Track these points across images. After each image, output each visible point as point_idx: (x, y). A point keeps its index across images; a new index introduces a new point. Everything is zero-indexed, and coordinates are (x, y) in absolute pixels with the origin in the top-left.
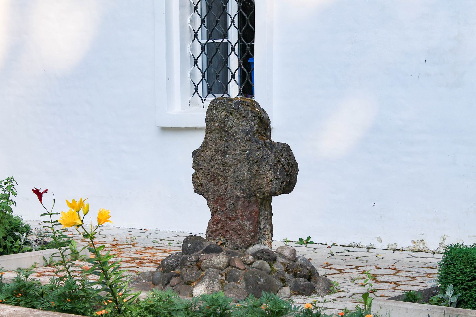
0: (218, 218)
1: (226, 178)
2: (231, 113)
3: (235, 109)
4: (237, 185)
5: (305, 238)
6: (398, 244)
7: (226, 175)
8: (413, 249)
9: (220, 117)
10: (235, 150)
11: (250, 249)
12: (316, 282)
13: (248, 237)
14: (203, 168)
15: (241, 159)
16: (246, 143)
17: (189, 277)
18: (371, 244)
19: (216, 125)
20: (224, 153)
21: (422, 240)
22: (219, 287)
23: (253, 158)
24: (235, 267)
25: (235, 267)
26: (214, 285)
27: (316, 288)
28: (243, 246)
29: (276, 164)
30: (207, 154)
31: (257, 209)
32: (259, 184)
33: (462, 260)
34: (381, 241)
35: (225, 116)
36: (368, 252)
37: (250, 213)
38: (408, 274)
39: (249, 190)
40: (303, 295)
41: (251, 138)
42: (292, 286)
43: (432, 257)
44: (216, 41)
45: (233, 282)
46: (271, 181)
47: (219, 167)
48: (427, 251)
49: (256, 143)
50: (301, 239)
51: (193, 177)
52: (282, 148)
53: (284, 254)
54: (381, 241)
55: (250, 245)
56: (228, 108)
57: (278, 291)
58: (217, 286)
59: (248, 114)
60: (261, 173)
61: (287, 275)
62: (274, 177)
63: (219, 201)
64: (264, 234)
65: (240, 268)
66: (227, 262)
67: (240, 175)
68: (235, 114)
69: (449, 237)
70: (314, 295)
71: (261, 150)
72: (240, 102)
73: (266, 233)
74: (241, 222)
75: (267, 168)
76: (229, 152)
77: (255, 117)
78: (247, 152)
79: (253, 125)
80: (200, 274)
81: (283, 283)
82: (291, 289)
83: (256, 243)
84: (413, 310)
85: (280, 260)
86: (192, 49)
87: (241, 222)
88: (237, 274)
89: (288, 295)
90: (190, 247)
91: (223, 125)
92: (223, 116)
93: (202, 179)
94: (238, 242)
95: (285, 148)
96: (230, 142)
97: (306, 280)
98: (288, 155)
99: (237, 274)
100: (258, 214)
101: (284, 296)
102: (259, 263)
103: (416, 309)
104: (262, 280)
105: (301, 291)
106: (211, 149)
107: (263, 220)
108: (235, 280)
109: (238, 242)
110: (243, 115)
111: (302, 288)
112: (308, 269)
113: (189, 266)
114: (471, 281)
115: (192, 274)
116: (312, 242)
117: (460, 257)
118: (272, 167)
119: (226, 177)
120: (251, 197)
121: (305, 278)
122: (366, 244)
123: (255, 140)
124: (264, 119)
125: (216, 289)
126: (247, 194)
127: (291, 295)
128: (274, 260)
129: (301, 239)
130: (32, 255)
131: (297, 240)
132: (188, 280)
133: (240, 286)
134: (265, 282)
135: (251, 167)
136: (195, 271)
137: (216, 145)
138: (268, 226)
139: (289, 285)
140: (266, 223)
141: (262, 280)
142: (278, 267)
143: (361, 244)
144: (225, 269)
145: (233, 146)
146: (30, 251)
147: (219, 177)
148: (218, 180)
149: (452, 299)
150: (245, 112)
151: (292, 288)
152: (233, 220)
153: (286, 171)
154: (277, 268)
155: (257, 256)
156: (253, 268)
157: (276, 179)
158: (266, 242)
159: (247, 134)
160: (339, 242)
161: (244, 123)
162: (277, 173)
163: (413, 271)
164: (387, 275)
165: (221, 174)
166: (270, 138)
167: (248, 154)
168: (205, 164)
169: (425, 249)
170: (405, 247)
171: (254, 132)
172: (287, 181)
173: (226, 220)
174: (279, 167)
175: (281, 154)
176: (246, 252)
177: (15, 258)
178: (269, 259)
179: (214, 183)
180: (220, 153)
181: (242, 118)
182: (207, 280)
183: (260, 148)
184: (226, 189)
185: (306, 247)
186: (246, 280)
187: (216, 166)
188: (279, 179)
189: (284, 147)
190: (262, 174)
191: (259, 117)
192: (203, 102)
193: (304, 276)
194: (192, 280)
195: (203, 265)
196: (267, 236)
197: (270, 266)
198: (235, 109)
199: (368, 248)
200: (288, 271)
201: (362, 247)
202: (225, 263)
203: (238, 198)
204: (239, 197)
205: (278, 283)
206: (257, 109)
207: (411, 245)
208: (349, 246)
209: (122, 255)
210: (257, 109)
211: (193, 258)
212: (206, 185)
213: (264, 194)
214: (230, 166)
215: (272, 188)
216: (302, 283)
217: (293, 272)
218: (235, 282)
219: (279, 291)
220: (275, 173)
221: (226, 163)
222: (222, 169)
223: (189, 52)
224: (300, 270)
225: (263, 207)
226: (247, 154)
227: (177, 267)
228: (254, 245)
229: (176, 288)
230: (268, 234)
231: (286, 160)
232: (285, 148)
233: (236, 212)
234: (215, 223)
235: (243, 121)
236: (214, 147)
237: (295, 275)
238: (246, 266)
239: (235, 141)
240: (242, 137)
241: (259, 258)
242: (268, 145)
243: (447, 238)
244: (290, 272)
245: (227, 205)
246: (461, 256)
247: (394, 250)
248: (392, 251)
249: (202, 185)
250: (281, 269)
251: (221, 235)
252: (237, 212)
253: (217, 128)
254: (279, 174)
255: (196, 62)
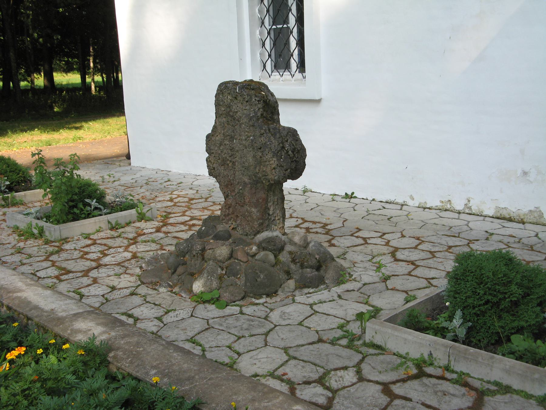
0: (229, 203)
1: (234, 163)
2: (236, 98)
3: (239, 94)
4: (244, 171)
5: (349, 193)
6: (428, 202)
7: (234, 160)
8: (441, 208)
9: (226, 101)
10: (240, 135)
11: (258, 236)
12: (326, 271)
13: (256, 224)
14: (214, 152)
15: (247, 145)
16: (250, 128)
17: (192, 268)
18: (404, 202)
19: (223, 109)
20: (232, 138)
21: (449, 201)
22: (217, 283)
23: (257, 143)
24: (238, 259)
25: (238, 259)
26: (211, 281)
27: (325, 277)
28: (251, 233)
29: (280, 151)
30: (217, 138)
31: (264, 196)
32: (264, 171)
33: (474, 275)
34: (413, 199)
35: (231, 100)
36: (401, 209)
37: (257, 200)
38: (429, 246)
39: (255, 176)
40: (309, 288)
41: (254, 123)
42: (297, 278)
43: (457, 218)
44: (278, 26)
45: (233, 277)
46: (274, 168)
47: (228, 152)
48: (453, 211)
49: (260, 128)
50: (346, 194)
51: (207, 160)
52: (288, 133)
53: (294, 240)
54: (413, 199)
55: (258, 232)
56: (232, 92)
57: (281, 285)
58: (215, 283)
59: (251, 98)
60: (265, 160)
61: (293, 266)
62: (277, 165)
63: (229, 187)
64: (274, 220)
65: (242, 260)
66: (229, 254)
67: (246, 161)
68: (239, 98)
69: (473, 199)
70: (322, 287)
71: (264, 136)
72: (244, 86)
73: (277, 218)
74: (249, 209)
75: (270, 155)
76: (236, 137)
77: (258, 101)
78: (251, 138)
79: (257, 109)
80: (203, 265)
81: (288, 275)
82: (296, 281)
83: (264, 230)
84: (413, 342)
85: (288, 248)
86: (261, 33)
87: (249, 209)
88: (238, 267)
89: (292, 289)
90: (203, 230)
91: (228, 110)
92: (229, 101)
93: (214, 163)
94: (247, 228)
95: (291, 132)
96: (236, 127)
97: (314, 270)
98: (294, 139)
99: (238, 267)
100: (266, 201)
101: (288, 290)
102: (262, 255)
103: (415, 342)
104: (262, 276)
105: (307, 284)
106: (220, 133)
107: (272, 206)
108: (235, 275)
109: (247, 228)
110: (246, 100)
111: (308, 280)
112: (316, 259)
113: (194, 256)
114: (484, 304)
115: (195, 265)
116: (355, 197)
117: (472, 272)
118: (275, 154)
119: (233, 162)
120: (257, 183)
121: (312, 269)
122: (401, 201)
123: (259, 126)
124: (271, 103)
125: (214, 285)
126: (254, 181)
127: (296, 289)
128: (282, 249)
129: (346, 194)
130: (97, 221)
131: (344, 194)
132: (191, 271)
133: (239, 283)
134: (265, 277)
135: (256, 153)
136: (199, 262)
137: (224, 130)
138: (278, 212)
139: (295, 277)
140: (275, 208)
141: (262, 276)
142: (284, 257)
143: (396, 201)
144: (226, 261)
145: (239, 131)
146: (101, 215)
147: (228, 162)
148: (228, 165)
149: (459, 329)
150: (248, 97)
151: (298, 280)
152: (242, 206)
153: (290, 158)
154: (283, 259)
155: (261, 247)
156: (256, 260)
157: (280, 167)
158: (276, 227)
159: (250, 119)
160: (378, 198)
161: (247, 108)
162: (280, 160)
163: (436, 241)
164: (409, 248)
165: (230, 159)
166: (279, 121)
167: (252, 140)
168: (216, 148)
169: (452, 209)
170: (434, 206)
171: (258, 117)
172: (292, 168)
173: (236, 206)
174: (283, 154)
175: (286, 139)
176: (254, 239)
177: (78, 224)
178: (274, 249)
179: (224, 167)
180: (228, 137)
181: (245, 102)
182: (205, 275)
183: (264, 134)
184: (234, 174)
185: (349, 202)
186: (246, 275)
187: (225, 151)
188: (282, 166)
189: (290, 132)
190: (266, 161)
191: (264, 101)
192: (270, 77)
193: (311, 267)
194: (195, 272)
195: (206, 256)
196: (278, 221)
197: (276, 257)
198: (239, 94)
199: (402, 205)
200: (295, 261)
201: (397, 204)
202: (226, 256)
203: (245, 184)
204: (246, 183)
205: (283, 276)
206: (263, 93)
207: (439, 204)
208: (387, 202)
209: (171, 221)
210: (263, 93)
211: (198, 247)
212: (217, 169)
213: (269, 181)
214: (237, 151)
215: (275, 176)
216: (309, 275)
217: (300, 263)
218: (234, 277)
219: (283, 286)
220: (278, 160)
221: (233, 148)
222: (230, 154)
223: (258, 36)
224: (308, 260)
225: (272, 193)
226: (251, 140)
227: (187, 253)
228: (262, 232)
229: (181, 278)
230: (279, 219)
231: (291, 146)
232: (291, 132)
233: (244, 199)
234: (227, 207)
235: (247, 106)
236: (222, 132)
237: (302, 266)
238: (249, 258)
239: (241, 125)
240: (246, 123)
241: (264, 249)
242: (271, 130)
243: (471, 200)
244: (297, 262)
245: (236, 191)
246: (474, 271)
247: (425, 208)
248: (422, 209)
249: (214, 169)
250: (287, 260)
251: (232, 219)
252: (245, 198)
253: (224, 112)
254: (283, 161)
255: (264, 45)
